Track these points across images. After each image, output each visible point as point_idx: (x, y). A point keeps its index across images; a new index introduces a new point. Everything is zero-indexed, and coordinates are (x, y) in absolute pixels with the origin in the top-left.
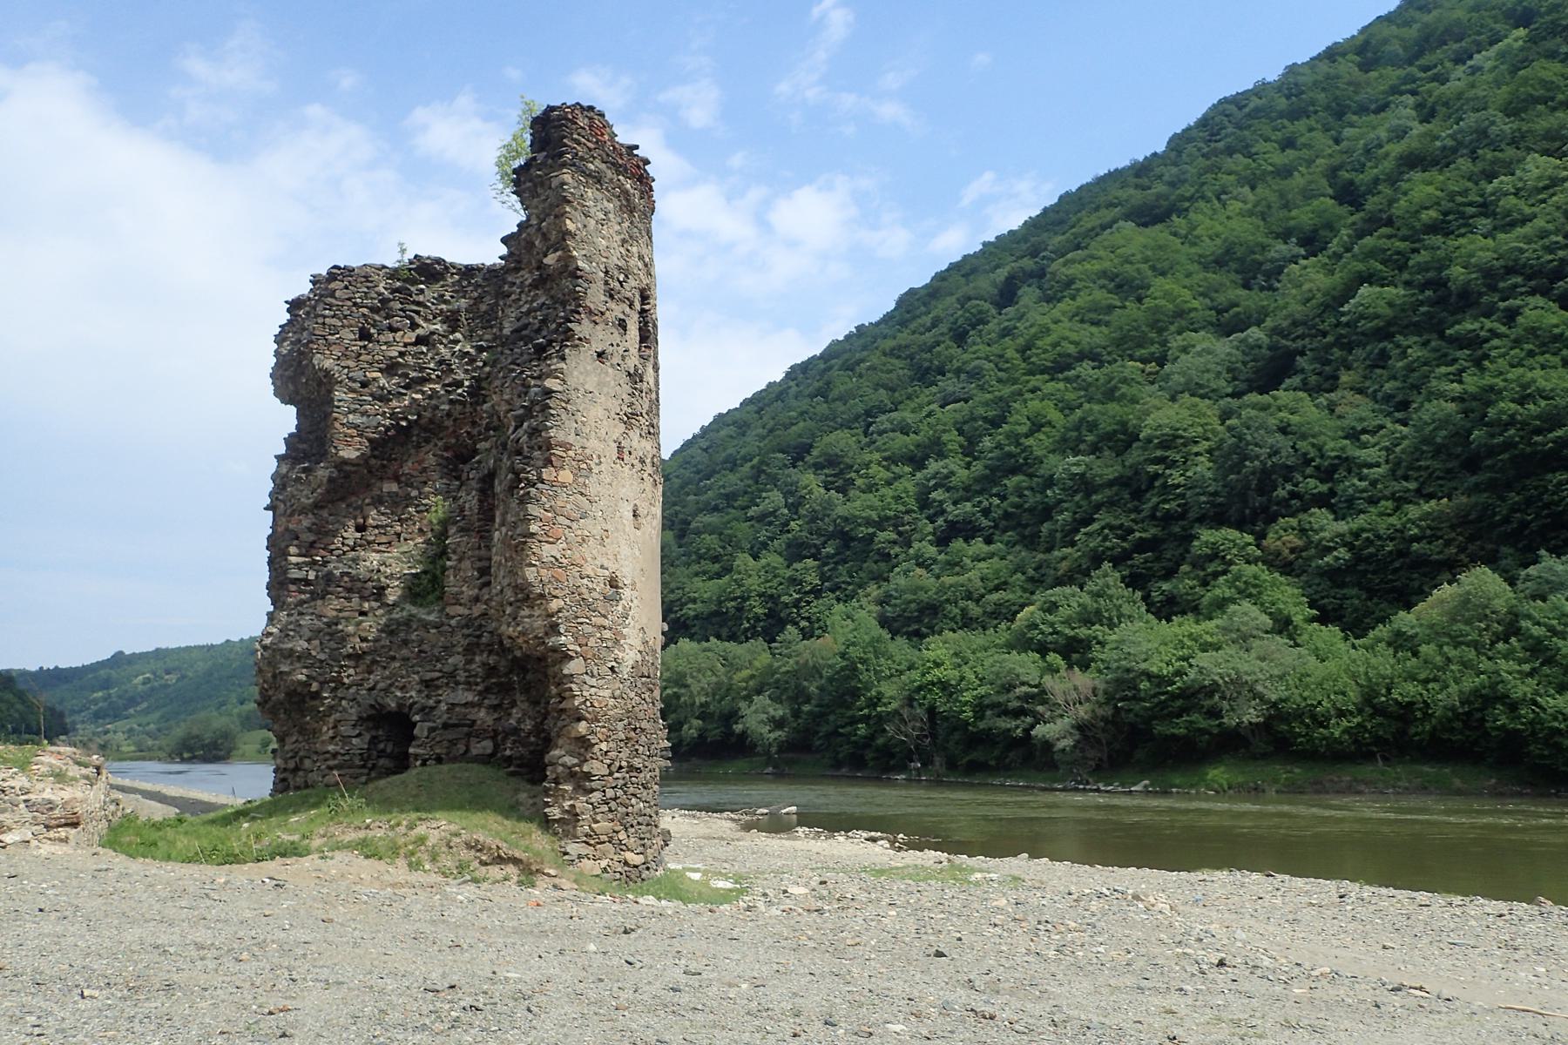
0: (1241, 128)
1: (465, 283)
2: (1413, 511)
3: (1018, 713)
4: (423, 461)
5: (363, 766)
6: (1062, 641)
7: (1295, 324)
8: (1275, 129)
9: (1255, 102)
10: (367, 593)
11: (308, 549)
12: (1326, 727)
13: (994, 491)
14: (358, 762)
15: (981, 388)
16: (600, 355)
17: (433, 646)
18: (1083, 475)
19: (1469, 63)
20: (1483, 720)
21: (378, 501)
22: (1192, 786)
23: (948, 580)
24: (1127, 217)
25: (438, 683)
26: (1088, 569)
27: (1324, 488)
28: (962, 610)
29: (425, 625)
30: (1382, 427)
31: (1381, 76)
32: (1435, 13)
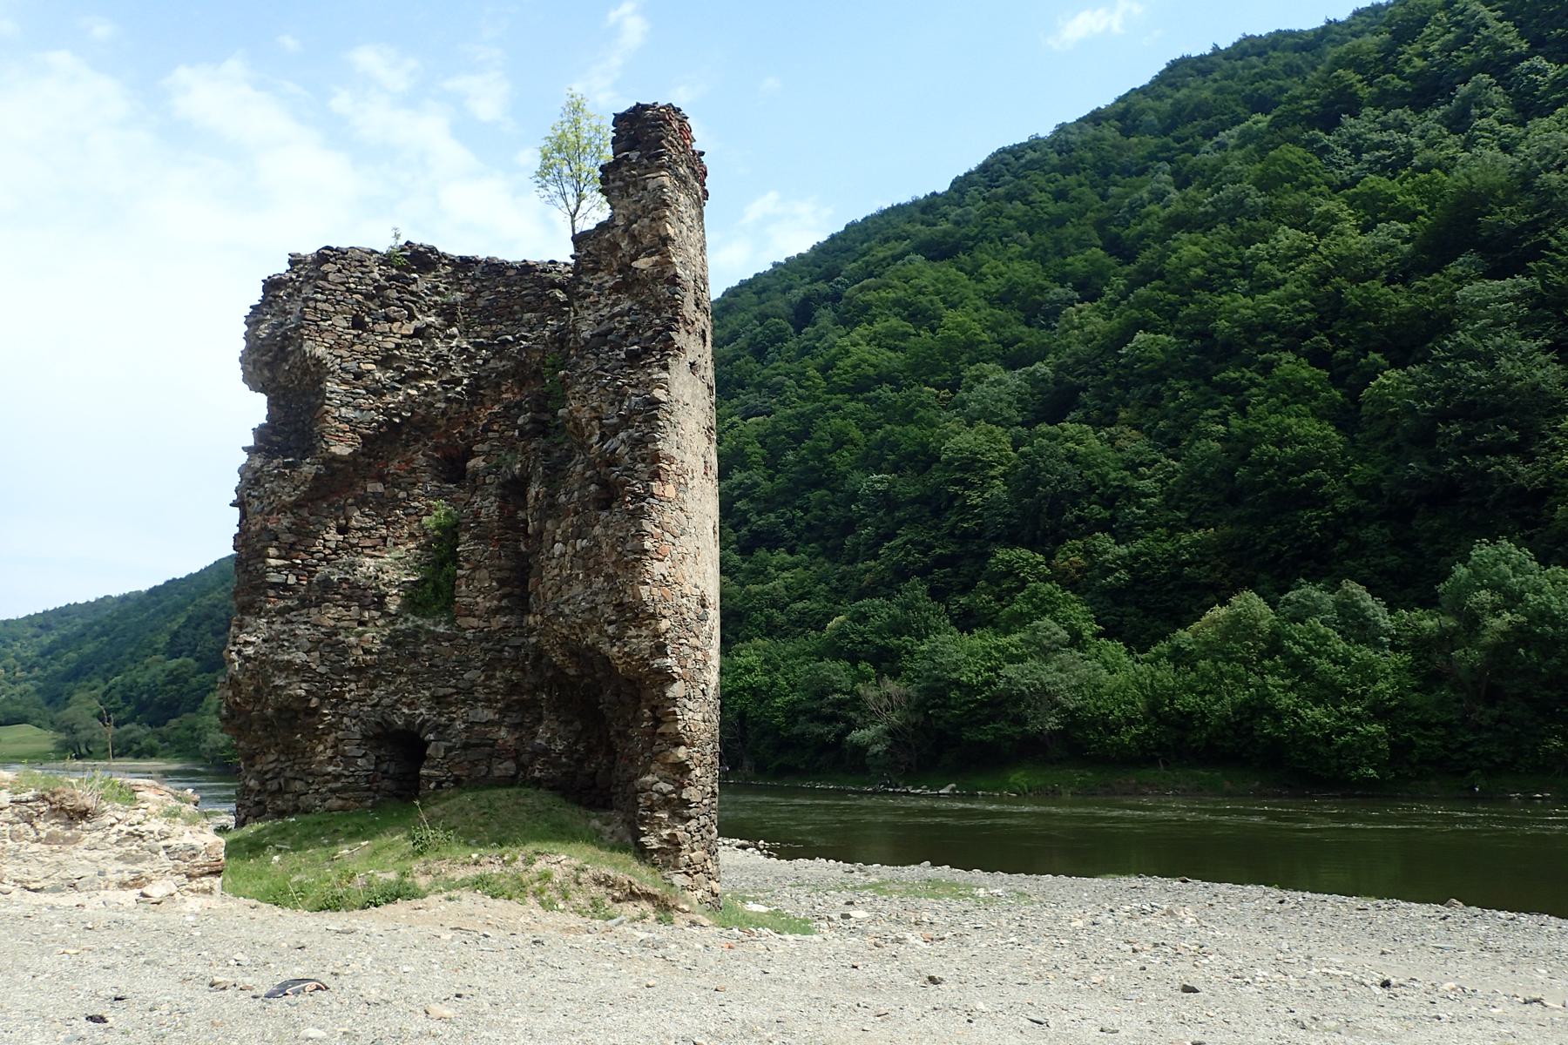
0: (1017, 177)
1: (461, 275)
2: (1185, 539)
3: (830, 719)
4: (412, 460)
5: (369, 789)
6: (872, 650)
7: (1078, 362)
8: (1049, 181)
9: (1030, 155)
10: (368, 601)
11: (287, 552)
12: (1117, 734)
13: (797, 503)
14: (364, 785)
15: (782, 403)
16: (692, 365)
17: (446, 660)
18: (885, 492)
19: (1216, 139)
20: (1252, 728)
21: (361, 502)
22: (995, 789)
23: (754, 588)
24: (917, 250)
25: (452, 699)
26: (891, 582)
27: (1106, 514)
28: (767, 617)
29: (436, 638)
30: (1156, 461)
31: (1140, 142)
32: (1185, 91)
